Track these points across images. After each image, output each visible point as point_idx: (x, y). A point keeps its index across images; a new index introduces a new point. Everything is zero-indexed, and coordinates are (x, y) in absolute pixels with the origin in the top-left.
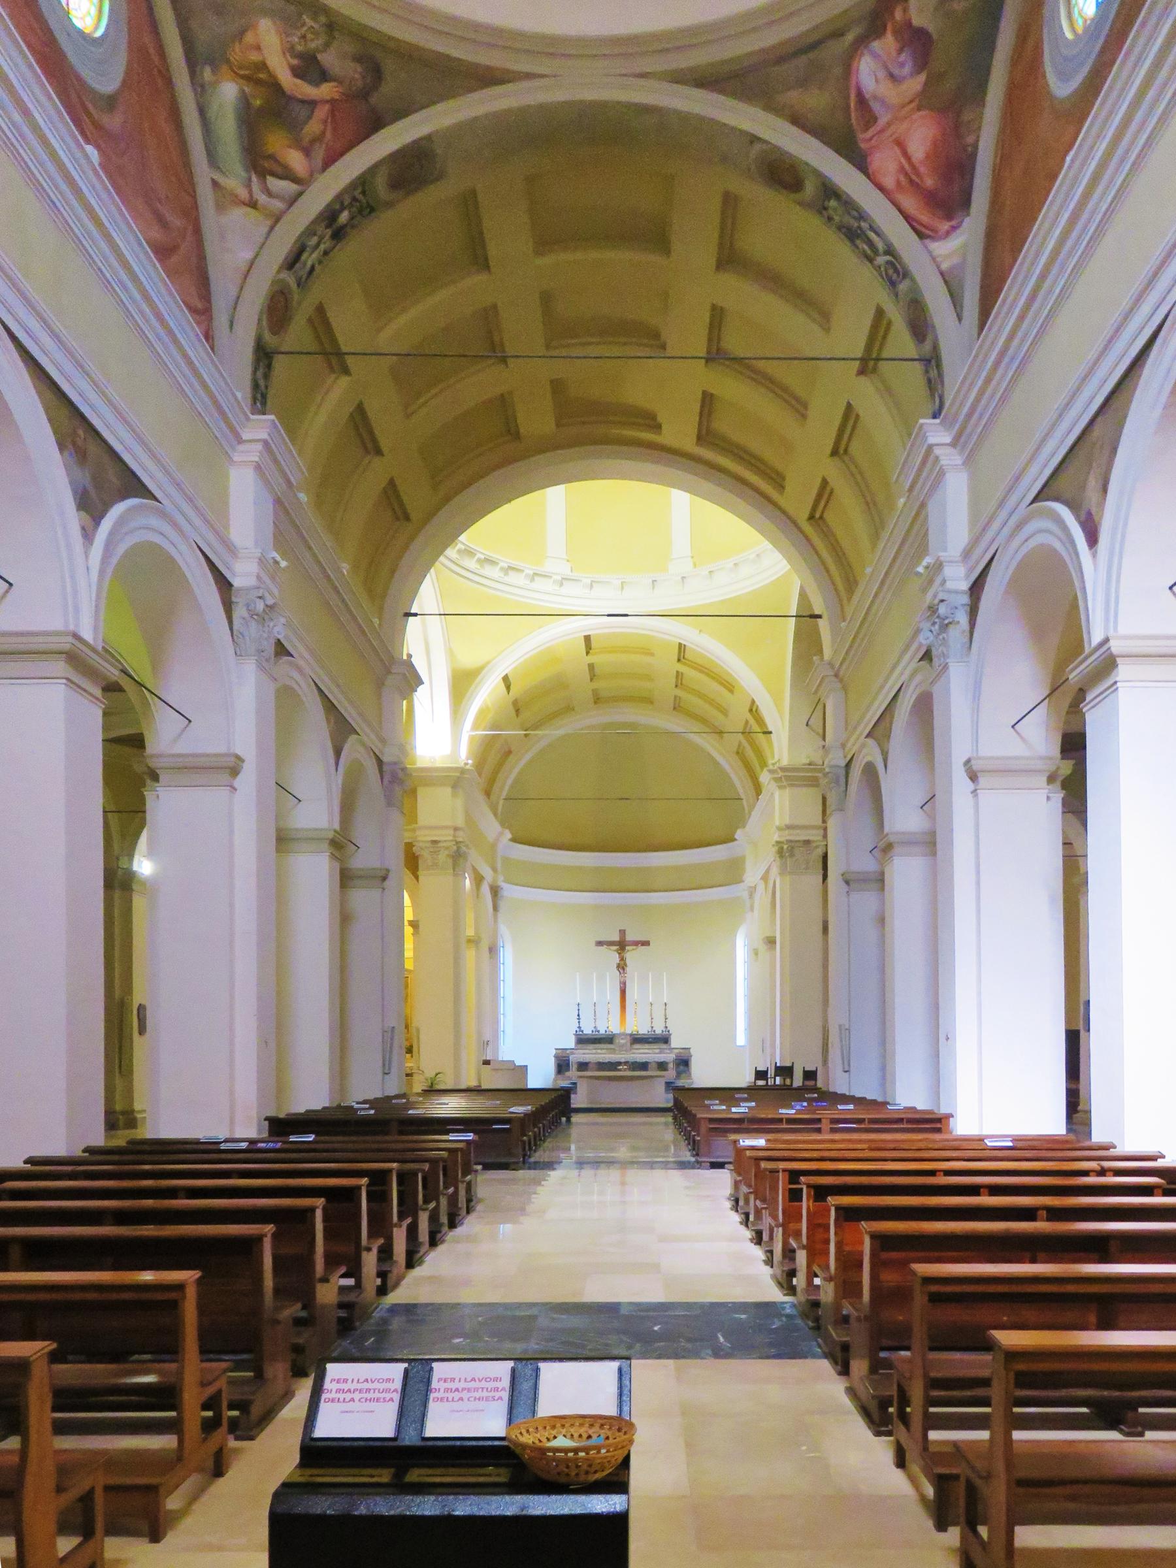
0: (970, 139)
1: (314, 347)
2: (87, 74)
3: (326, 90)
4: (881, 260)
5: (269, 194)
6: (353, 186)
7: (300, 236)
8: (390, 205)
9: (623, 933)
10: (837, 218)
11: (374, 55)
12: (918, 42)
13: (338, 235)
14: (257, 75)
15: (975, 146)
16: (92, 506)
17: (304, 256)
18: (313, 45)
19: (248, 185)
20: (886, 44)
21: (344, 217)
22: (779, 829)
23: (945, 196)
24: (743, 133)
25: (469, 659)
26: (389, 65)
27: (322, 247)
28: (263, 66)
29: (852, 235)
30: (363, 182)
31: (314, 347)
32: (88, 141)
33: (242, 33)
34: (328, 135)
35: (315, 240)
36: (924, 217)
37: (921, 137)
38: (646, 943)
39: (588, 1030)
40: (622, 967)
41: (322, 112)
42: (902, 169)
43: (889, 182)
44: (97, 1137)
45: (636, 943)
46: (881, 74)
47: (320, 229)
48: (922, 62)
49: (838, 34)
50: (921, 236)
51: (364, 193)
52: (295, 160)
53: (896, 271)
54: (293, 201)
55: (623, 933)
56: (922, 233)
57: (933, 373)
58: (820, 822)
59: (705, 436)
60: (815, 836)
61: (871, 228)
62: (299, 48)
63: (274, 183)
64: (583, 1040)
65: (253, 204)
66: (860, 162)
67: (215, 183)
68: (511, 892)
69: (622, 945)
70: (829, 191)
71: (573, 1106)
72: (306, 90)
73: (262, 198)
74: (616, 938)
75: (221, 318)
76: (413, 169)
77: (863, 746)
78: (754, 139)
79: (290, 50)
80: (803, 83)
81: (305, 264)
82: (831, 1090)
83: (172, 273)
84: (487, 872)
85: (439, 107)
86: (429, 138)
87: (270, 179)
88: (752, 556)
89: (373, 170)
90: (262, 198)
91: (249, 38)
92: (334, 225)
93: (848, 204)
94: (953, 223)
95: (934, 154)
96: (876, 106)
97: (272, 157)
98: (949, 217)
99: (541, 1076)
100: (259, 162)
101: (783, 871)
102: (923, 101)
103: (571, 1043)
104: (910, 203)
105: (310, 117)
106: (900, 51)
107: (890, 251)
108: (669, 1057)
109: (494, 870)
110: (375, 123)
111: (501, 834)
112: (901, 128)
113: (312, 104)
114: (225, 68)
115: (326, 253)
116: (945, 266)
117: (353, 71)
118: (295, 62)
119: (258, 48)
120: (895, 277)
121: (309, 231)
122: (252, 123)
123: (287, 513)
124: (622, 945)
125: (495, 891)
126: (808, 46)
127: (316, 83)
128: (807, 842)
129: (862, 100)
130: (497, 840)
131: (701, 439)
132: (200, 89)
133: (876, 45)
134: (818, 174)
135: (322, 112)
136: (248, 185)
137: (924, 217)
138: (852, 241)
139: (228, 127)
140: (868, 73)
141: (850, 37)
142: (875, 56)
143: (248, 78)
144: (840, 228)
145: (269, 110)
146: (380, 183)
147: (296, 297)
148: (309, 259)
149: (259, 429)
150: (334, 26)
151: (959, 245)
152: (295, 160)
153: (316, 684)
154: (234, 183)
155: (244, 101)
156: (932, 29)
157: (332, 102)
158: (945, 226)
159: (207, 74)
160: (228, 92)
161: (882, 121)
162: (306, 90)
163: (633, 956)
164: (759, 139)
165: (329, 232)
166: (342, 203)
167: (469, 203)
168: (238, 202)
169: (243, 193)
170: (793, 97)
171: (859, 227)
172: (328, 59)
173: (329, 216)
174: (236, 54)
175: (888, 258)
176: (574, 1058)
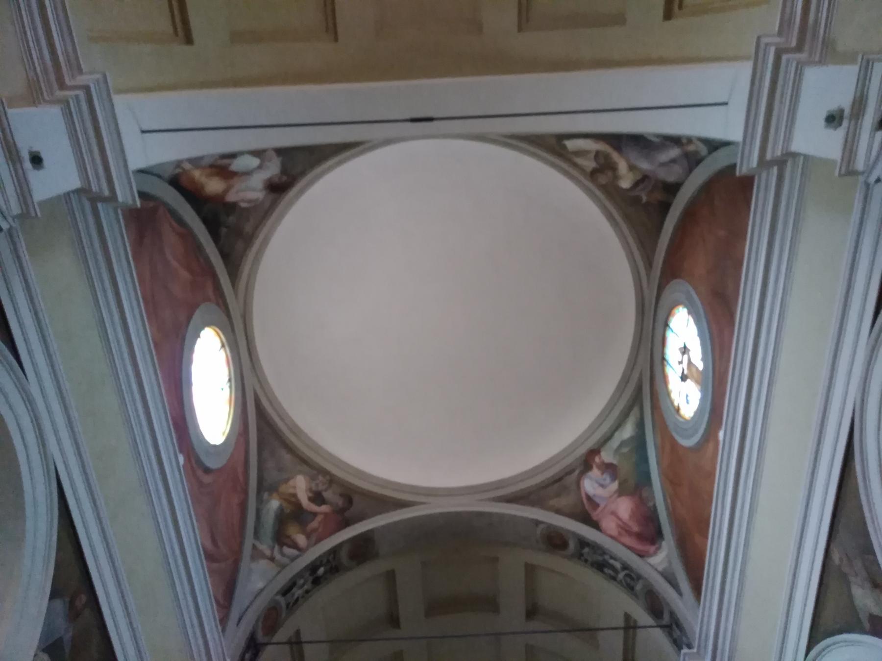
3: (324, 508)
4: (621, 576)
5: (283, 555)
7: (294, 576)
8: (349, 569)
10: (590, 559)
12: (609, 468)
15: (655, 506)
17: (295, 589)
19: (272, 549)
20: (595, 472)
21: (321, 570)
23: (649, 533)
24: (532, 520)
26: (356, 499)
27: (306, 587)
28: (294, 495)
29: (600, 566)
30: (334, 551)
32: (181, 451)
34: (320, 530)
35: (302, 581)
36: (639, 547)
37: (625, 508)
42: (619, 526)
46: (596, 485)
47: (307, 574)
48: (614, 478)
51: (334, 558)
52: (301, 540)
53: (632, 579)
54: (293, 559)
56: (642, 555)
57: (677, 633)
61: (612, 558)
62: (314, 489)
63: (288, 551)
65: (272, 559)
66: (596, 525)
70: (583, 543)
72: (314, 508)
75: (235, 614)
76: (363, 549)
78: (537, 523)
79: (310, 490)
80: (558, 495)
81: (293, 595)
83: (212, 572)
85: (379, 517)
89: (340, 546)
90: (278, 556)
91: (291, 483)
94: (657, 546)
95: (633, 515)
96: (597, 500)
97: (289, 537)
100: (281, 538)
102: (621, 492)
104: (628, 540)
105: (313, 520)
106: (602, 474)
107: (625, 567)
110: (346, 523)
113: (315, 514)
114: (275, 495)
115: (307, 592)
116: (660, 569)
117: (340, 502)
118: (311, 495)
119: (295, 487)
120: (632, 583)
121: (300, 575)
122: (282, 519)
126: (558, 479)
127: (320, 505)
129: (589, 498)
132: (260, 501)
133: (590, 474)
135: (319, 518)
136: (272, 549)
137: (639, 547)
138: (602, 571)
139: (269, 519)
141: (577, 472)
143: (285, 500)
145: (294, 514)
146: (344, 555)
147: (284, 615)
148: (297, 592)
151: (664, 556)
153: (25, 375)
155: (281, 509)
156: (615, 462)
157: (326, 514)
158: (652, 549)
159: (266, 495)
160: (274, 504)
161: (602, 505)
162: (314, 508)
164: (542, 522)
165: (311, 579)
166: (321, 562)
167: (390, 577)
168: (263, 556)
169: (268, 553)
170: (553, 502)
171: (604, 560)
172: (327, 495)
173: (313, 568)
174: (283, 488)
175: (626, 572)
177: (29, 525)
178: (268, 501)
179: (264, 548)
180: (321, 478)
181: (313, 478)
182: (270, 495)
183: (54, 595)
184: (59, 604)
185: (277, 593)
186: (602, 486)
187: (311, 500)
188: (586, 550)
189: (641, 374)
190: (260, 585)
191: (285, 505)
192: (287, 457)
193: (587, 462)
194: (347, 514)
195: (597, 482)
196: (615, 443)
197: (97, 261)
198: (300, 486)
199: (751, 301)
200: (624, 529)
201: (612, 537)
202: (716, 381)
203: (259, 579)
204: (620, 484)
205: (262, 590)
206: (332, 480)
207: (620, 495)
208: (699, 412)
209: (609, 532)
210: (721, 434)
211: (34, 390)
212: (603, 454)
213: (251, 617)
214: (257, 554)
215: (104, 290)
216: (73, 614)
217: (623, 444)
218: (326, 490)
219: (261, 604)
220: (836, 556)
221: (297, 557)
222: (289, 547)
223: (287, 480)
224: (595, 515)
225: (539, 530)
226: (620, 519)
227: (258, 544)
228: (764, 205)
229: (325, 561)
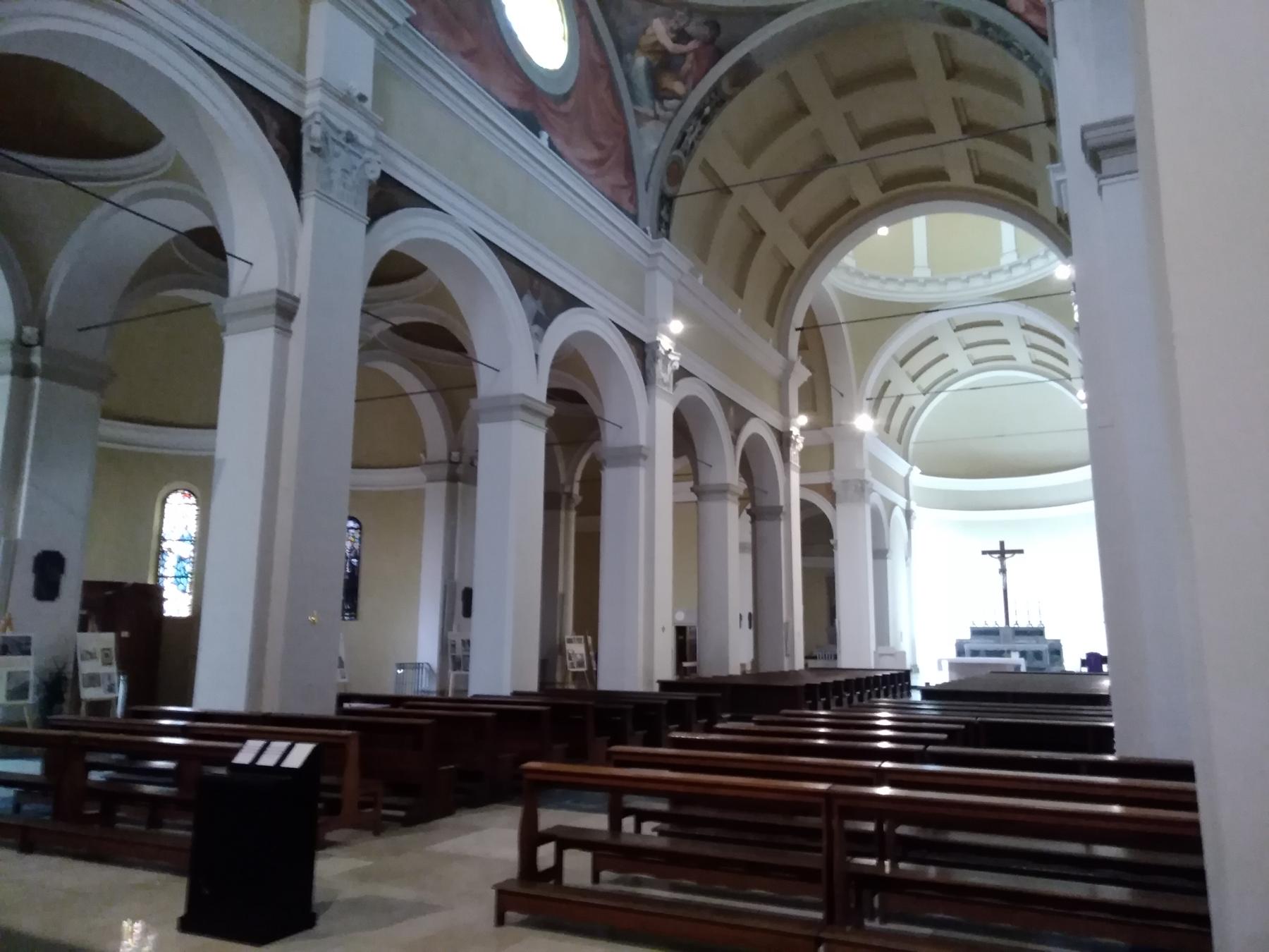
1: (708, 186)
3: (692, 45)
5: (666, 110)
6: (709, 93)
8: (731, 98)
9: (1002, 544)
11: (714, 19)
13: (706, 121)
14: (656, 48)
16: (542, 321)
18: (682, 24)
19: (654, 108)
21: (707, 110)
28: (657, 43)
30: (716, 89)
31: (708, 186)
33: (645, 30)
38: (1021, 552)
40: (1003, 571)
41: (690, 57)
44: (532, 685)
45: (1013, 552)
52: (678, 87)
54: (676, 111)
55: (1002, 544)
59: (981, 178)
62: (675, 28)
63: (672, 103)
65: (657, 117)
67: (636, 113)
71: (532, 685)
72: (682, 48)
73: (661, 112)
74: (998, 548)
76: (744, 73)
79: (672, 31)
86: (748, 54)
88: (986, 273)
90: (661, 112)
91: (649, 31)
92: (702, 118)
93: (999, 29)
97: (666, 89)
100: (659, 93)
108: (1043, 647)
109: (907, 497)
110: (719, 54)
113: (684, 55)
115: (700, 133)
117: (705, 31)
119: (654, 34)
121: (688, 124)
122: (653, 74)
125: (908, 514)
127: (685, 43)
131: (978, 179)
134: (977, 16)
135: (690, 57)
136: (654, 108)
139: (641, 81)
143: (649, 52)
145: (664, 63)
148: (689, 139)
149: (666, 246)
150: (692, 11)
152: (678, 87)
154: (646, 109)
155: (649, 63)
160: (640, 61)
162: (682, 48)
163: (1010, 561)
165: (699, 122)
167: (785, 78)
168: (648, 118)
169: (651, 113)
172: (691, 29)
173: (698, 113)
174: (646, 41)
176: (966, 647)
178: (633, 61)
179: (646, 109)
180: (679, 13)
182: (633, 54)
183: (521, 296)
184: (527, 297)
185: (672, 150)
187: (675, 41)
188: (990, 30)
190: (654, 146)
191: (651, 58)
197: (411, 67)
198: (659, 30)
201: (1017, 15)
203: (649, 142)
205: (657, 151)
209: (1015, 8)
213: (655, 179)
214: (641, 118)
216: (536, 295)
218: (688, 24)
219: (661, 163)
221: (680, 107)
222: (671, 99)
223: (644, 32)
225: (938, 8)
227: (640, 109)
229: (708, 101)
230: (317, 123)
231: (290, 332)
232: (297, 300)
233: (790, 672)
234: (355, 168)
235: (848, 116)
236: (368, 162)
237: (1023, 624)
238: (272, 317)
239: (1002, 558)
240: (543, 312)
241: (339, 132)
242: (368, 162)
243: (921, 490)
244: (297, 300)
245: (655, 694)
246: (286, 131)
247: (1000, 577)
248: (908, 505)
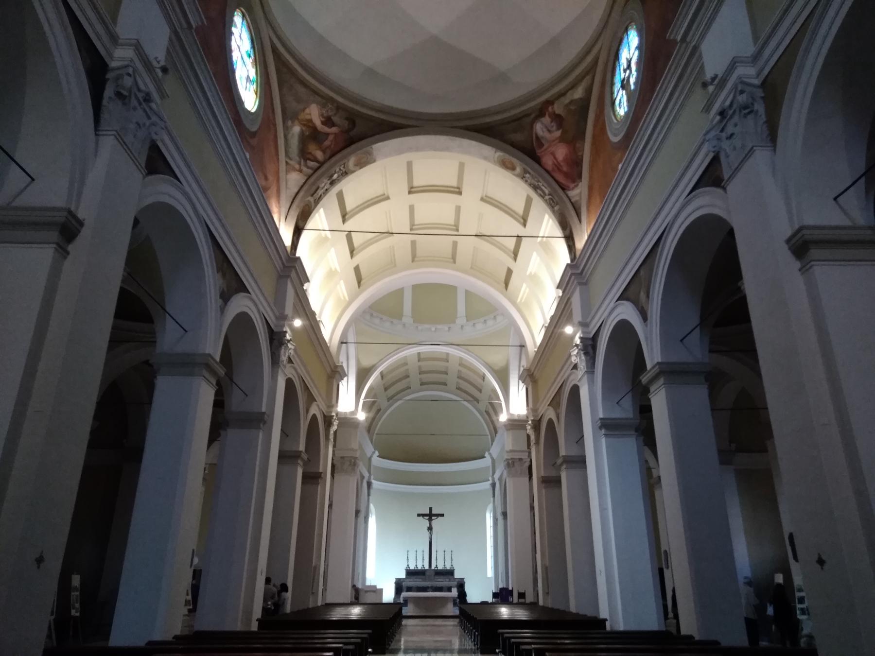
0: (580, 154)
2: (248, 125)
3: (334, 130)
5: (308, 167)
8: (353, 172)
9: (431, 509)
12: (558, 119)
14: (308, 124)
15: (582, 156)
19: (300, 164)
20: (546, 120)
21: (335, 176)
22: (507, 452)
25: (366, 363)
28: (311, 121)
37: (562, 152)
38: (442, 515)
39: (412, 567)
40: (430, 529)
41: (331, 137)
42: (554, 164)
43: (550, 168)
46: (545, 130)
49: (528, 115)
50: (563, 189)
52: (319, 155)
55: (431, 509)
58: (526, 448)
60: (525, 456)
64: (410, 573)
65: (301, 171)
68: (376, 484)
69: (430, 516)
72: (326, 129)
74: (428, 512)
77: (547, 410)
79: (322, 115)
82: (201, 352)
84: (366, 475)
87: (308, 162)
91: (307, 111)
95: (565, 160)
96: (543, 142)
97: (310, 153)
98: (574, 182)
99: (388, 596)
100: (304, 155)
101: (509, 474)
102: (562, 139)
103: (403, 575)
105: (327, 139)
111: (374, 453)
112: (552, 149)
113: (328, 134)
114: (296, 122)
117: (346, 124)
122: (304, 140)
123: (300, 301)
124: (430, 516)
125: (369, 484)
126: (518, 119)
127: (330, 127)
128: (521, 459)
129: (537, 138)
130: (371, 457)
132: (286, 129)
133: (543, 119)
135: (331, 137)
139: (294, 143)
140: (539, 128)
141: (533, 116)
142: (542, 124)
143: (304, 125)
144: (530, 185)
152: (319, 155)
155: (302, 133)
158: (572, 185)
159: (290, 123)
160: (297, 129)
162: (326, 129)
163: (436, 522)
168: (294, 170)
172: (335, 119)
174: (302, 116)
177: (202, 252)
178: (292, 127)
181: (323, 106)
182: (293, 122)
186: (549, 131)
187: (323, 123)
189: (600, 50)
192: (301, 90)
193: (541, 112)
194: (352, 134)
195: (546, 127)
196: (566, 100)
198: (315, 113)
199: (643, 135)
200: (558, 167)
202: (642, 98)
204: (562, 133)
206: (339, 107)
207: (560, 142)
208: (627, 114)
210: (620, 166)
211: (188, 189)
212: (556, 106)
214: (289, 168)
215: (191, 83)
217: (571, 102)
220: (642, 272)
221: (319, 168)
223: (304, 110)
224: (539, 152)
226: (555, 158)
228: (676, 68)
230: (129, 75)
231: (68, 253)
232: (81, 224)
233: (313, 608)
234: (144, 125)
235: (412, 208)
236: (154, 124)
237: (440, 567)
238: (54, 235)
239: (430, 520)
240: (225, 289)
241: (139, 90)
242: (154, 124)
243: (377, 468)
244: (81, 224)
245: (254, 632)
246: (97, 71)
247: (427, 533)
248: (369, 477)
